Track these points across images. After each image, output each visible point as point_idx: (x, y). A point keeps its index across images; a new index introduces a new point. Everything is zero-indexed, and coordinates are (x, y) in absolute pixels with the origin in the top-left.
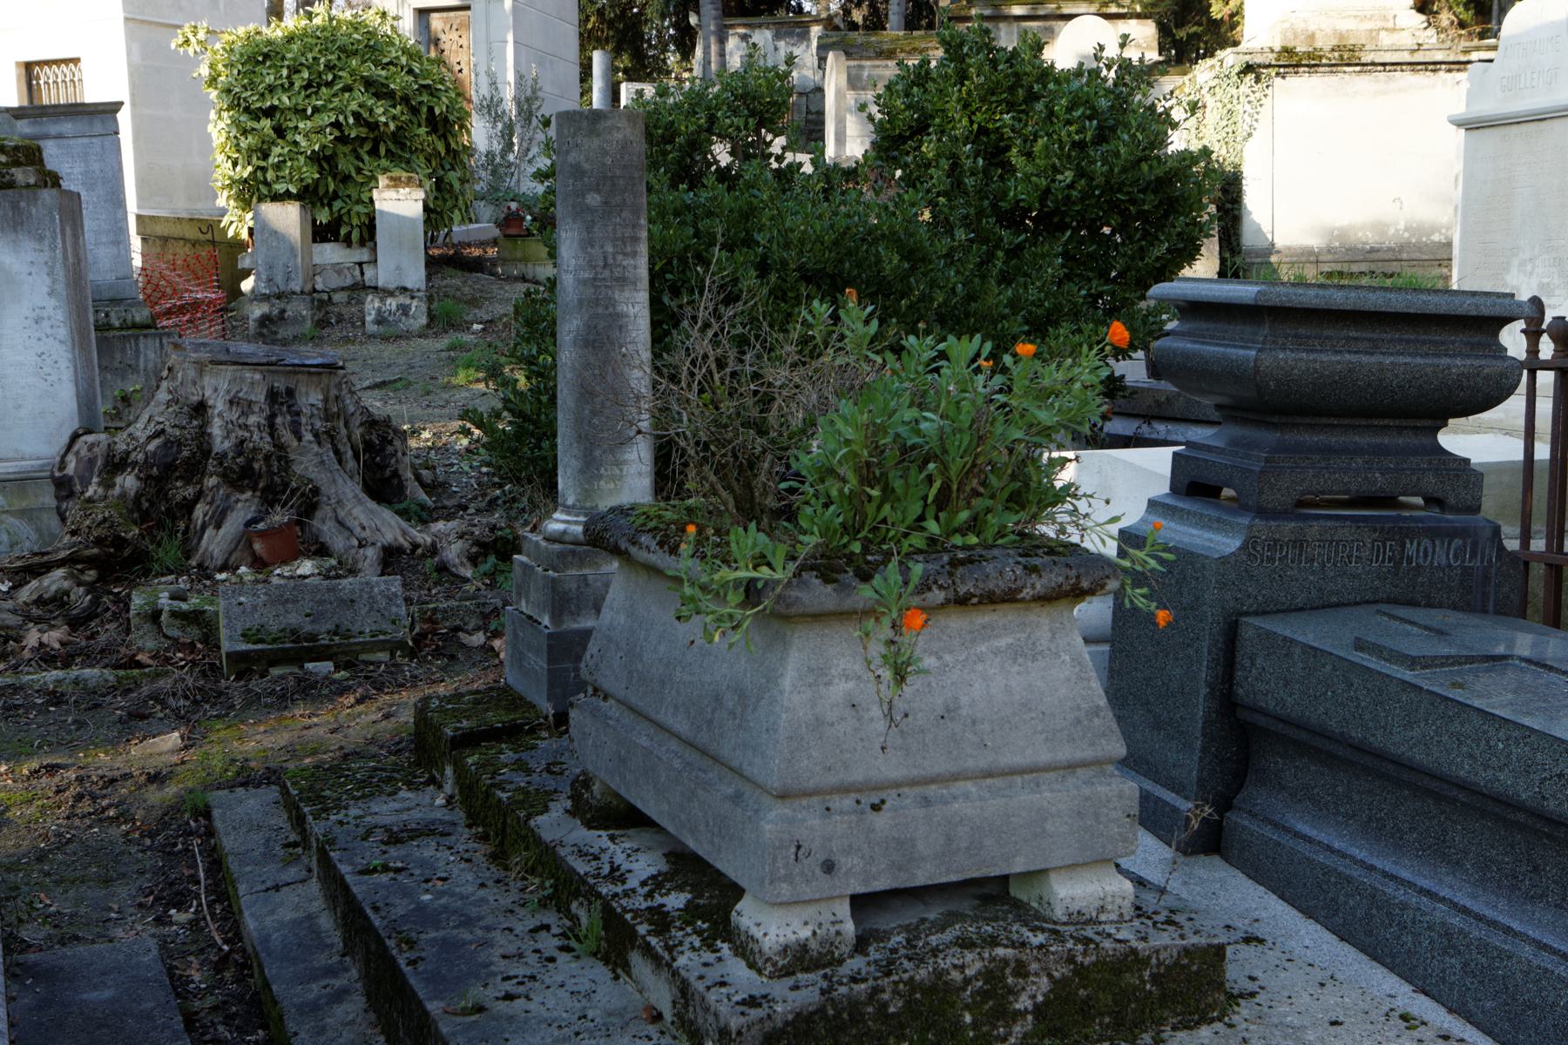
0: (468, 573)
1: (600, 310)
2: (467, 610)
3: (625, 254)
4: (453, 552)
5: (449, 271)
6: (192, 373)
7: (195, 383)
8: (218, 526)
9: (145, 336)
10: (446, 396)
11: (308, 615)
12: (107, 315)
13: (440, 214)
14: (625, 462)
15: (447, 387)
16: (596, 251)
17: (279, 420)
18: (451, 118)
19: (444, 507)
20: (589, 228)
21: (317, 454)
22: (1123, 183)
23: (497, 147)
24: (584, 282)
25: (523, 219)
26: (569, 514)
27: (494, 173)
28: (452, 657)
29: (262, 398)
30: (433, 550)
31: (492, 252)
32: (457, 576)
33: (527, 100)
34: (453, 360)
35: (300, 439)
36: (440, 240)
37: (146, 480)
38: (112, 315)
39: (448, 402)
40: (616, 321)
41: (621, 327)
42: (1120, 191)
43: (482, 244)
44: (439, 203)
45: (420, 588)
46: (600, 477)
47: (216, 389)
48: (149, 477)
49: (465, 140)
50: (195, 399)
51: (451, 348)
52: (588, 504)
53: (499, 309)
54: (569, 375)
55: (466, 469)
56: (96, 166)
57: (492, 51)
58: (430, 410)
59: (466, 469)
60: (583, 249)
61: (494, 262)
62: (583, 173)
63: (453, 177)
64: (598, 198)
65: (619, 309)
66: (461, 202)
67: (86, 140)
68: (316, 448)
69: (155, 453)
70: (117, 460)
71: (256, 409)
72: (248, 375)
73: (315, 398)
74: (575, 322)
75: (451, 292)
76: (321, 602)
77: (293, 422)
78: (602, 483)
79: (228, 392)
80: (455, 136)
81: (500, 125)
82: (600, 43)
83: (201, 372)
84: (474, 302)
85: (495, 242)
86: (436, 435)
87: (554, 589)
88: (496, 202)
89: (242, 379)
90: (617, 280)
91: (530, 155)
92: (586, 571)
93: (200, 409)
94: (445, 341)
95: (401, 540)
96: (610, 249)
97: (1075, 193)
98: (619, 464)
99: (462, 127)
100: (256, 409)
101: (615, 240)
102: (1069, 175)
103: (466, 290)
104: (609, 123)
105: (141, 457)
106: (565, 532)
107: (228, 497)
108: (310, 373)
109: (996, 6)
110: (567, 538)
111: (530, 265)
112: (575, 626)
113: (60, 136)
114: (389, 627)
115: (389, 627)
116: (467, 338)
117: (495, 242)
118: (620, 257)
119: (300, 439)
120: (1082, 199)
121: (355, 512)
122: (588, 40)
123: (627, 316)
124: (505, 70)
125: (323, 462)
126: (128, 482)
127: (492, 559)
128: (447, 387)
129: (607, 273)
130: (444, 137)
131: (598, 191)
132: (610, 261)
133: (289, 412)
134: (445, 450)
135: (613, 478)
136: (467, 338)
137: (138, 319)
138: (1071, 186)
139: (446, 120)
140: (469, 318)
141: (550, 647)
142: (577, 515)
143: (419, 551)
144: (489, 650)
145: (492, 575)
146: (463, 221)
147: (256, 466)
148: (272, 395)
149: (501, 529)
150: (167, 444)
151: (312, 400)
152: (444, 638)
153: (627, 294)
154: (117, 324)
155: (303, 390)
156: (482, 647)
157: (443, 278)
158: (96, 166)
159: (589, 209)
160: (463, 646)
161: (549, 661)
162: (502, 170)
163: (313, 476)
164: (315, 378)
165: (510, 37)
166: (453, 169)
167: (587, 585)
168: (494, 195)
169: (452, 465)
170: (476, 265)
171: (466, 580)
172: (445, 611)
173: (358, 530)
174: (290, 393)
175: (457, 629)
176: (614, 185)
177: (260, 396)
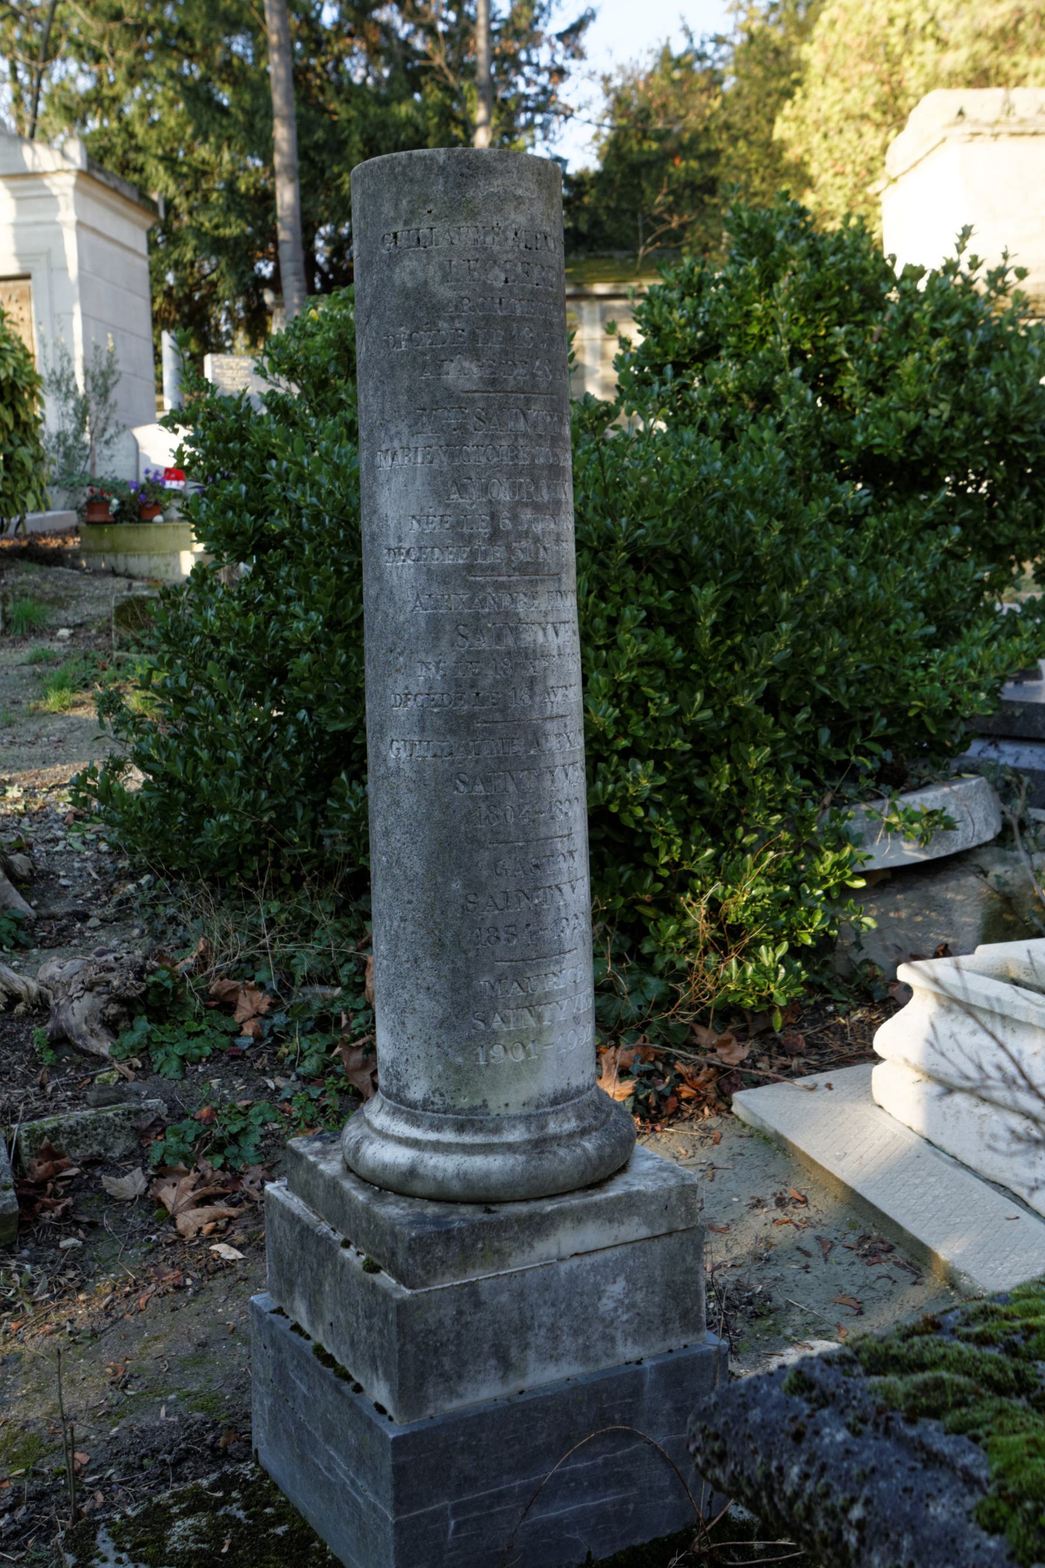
0: (103, 1046)
1: (484, 644)
2: (111, 1127)
3: (538, 508)
4: (77, 1013)
5: (23, 565)
10: (34, 728)
13: (11, 498)
14: (547, 998)
15: (35, 714)
16: (471, 501)
18: (20, 383)
19: (53, 917)
20: (454, 444)
22: (1022, 419)
23: (70, 427)
24: (444, 577)
25: (108, 503)
26: (414, 1121)
27: (66, 455)
28: (93, 1226)
30: (41, 1007)
31: (73, 543)
32: (85, 1053)
33: (102, 374)
34: (40, 677)
36: (11, 530)
39: (38, 737)
40: (522, 664)
41: (532, 682)
42: (1018, 430)
43: (57, 534)
44: (9, 484)
45: (26, 1080)
46: (491, 1038)
49: (37, 411)
51: (36, 660)
52: (464, 1102)
53: (89, 609)
54: (408, 800)
55: (77, 845)
57: (58, 320)
58: (15, 750)
59: (77, 845)
60: (439, 494)
61: (76, 554)
62: (435, 309)
63: (24, 453)
64: (474, 369)
65: (527, 638)
66: (35, 484)
74: (421, 674)
75: (29, 590)
78: (497, 1050)
80: (24, 405)
81: (72, 403)
82: (168, 325)
84: (58, 602)
85: (76, 531)
86: (30, 792)
87: (401, 1327)
88: (72, 488)
90: (522, 569)
91: (107, 436)
94: (26, 652)
96: (504, 495)
97: (957, 434)
98: (532, 1004)
99: (33, 394)
101: (514, 472)
102: (945, 409)
103: (47, 587)
104: (497, 185)
106: (412, 1172)
109: (578, 285)
110: (417, 1186)
111: (121, 557)
112: (453, 1405)
116: (56, 646)
117: (76, 531)
118: (527, 515)
120: (965, 444)
122: (159, 321)
123: (545, 656)
124: (73, 345)
127: (142, 1024)
128: (35, 714)
129: (499, 553)
130: (11, 406)
131: (476, 355)
132: (506, 524)
134: (43, 816)
136: (56, 646)
138: (951, 423)
139: (13, 386)
140: (53, 621)
141: (399, 1470)
142: (438, 1128)
143: (20, 1008)
144: (152, 1203)
145: (144, 1051)
146: (38, 508)
149: (153, 972)
152: (74, 1186)
153: (542, 603)
156: (143, 1197)
157: (19, 574)
159: (455, 399)
160: (110, 1199)
161: (400, 1503)
162: (76, 453)
165: (77, 309)
166: (24, 444)
167: (478, 1304)
168: (68, 482)
169: (56, 840)
170: (55, 558)
171: (101, 1061)
172: (73, 1131)
175: (93, 1162)
176: (509, 339)
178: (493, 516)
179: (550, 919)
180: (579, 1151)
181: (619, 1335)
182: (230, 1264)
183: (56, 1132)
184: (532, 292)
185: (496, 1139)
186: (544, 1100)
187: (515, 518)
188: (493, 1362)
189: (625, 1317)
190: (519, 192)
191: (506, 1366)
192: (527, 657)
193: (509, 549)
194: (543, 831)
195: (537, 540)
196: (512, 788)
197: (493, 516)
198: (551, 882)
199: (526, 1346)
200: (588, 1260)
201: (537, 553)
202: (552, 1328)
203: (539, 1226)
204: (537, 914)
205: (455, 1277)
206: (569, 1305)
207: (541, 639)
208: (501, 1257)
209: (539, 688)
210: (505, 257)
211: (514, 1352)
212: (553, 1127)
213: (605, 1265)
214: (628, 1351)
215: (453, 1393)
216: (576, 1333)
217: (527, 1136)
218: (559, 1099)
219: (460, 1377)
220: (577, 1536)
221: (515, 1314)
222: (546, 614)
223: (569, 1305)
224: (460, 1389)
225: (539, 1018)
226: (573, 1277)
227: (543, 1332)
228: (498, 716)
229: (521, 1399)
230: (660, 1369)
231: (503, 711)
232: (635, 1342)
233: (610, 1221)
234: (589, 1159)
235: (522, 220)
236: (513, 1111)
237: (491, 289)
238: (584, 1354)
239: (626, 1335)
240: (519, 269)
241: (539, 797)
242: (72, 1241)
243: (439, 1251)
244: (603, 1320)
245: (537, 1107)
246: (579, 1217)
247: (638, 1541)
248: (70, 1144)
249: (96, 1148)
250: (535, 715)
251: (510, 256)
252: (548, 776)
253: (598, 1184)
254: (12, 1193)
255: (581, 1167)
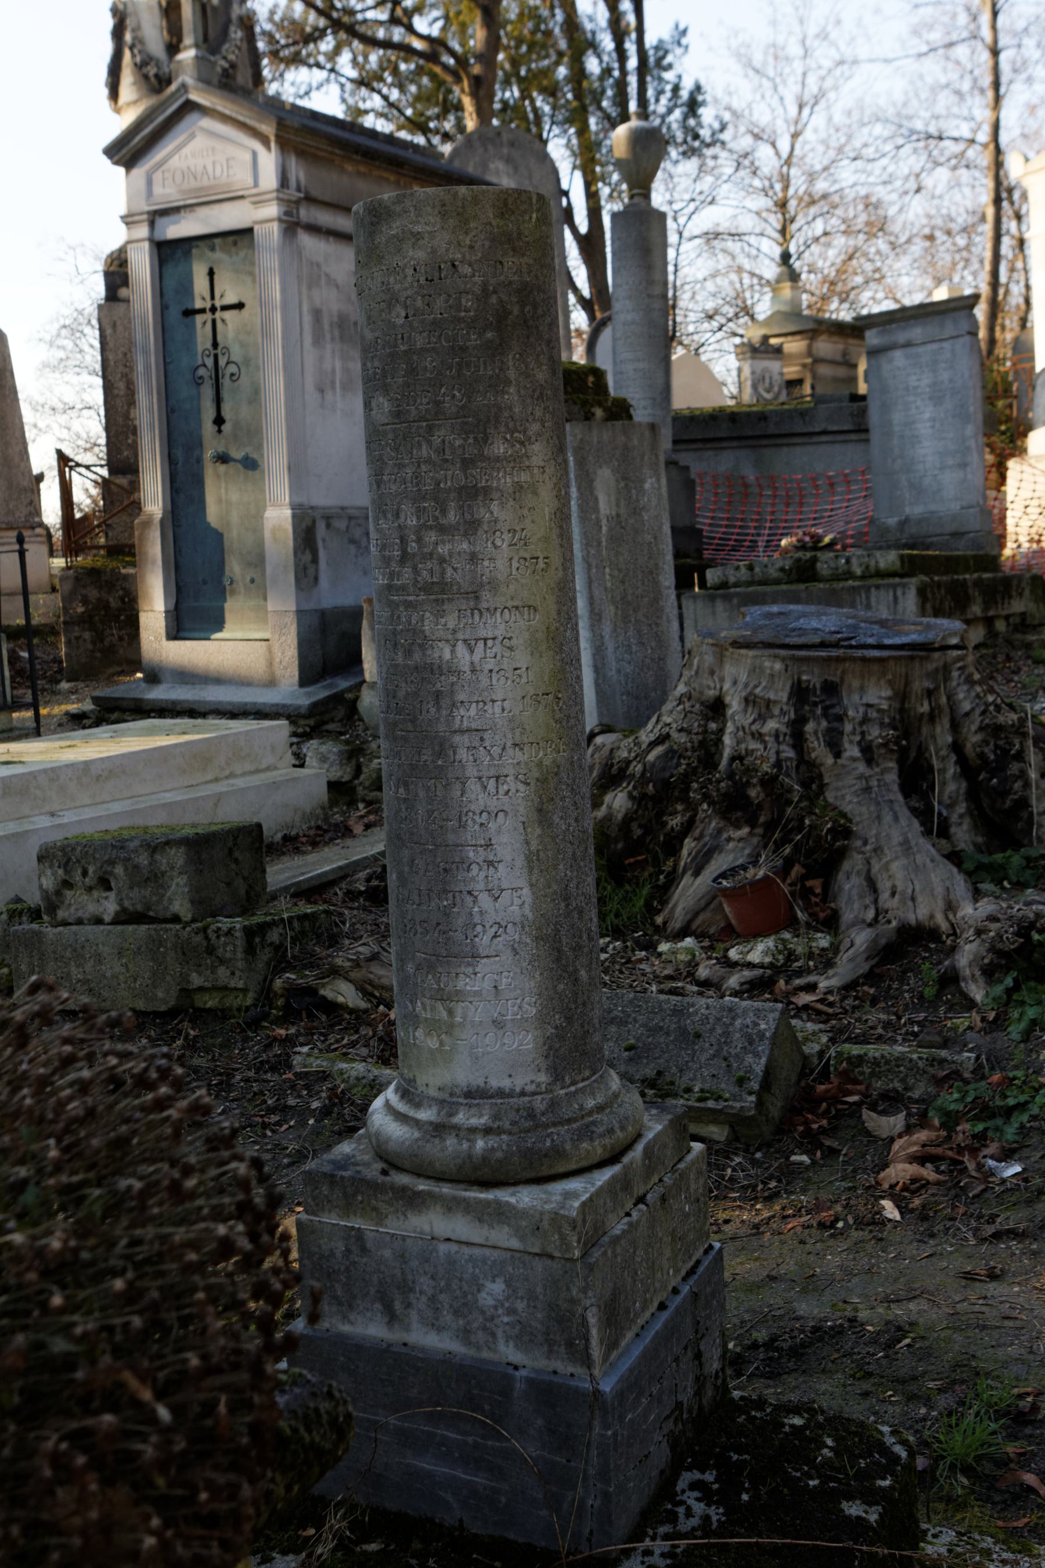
2: (912, 1066)
3: (442, 529)
6: (709, 659)
7: (712, 673)
8: (697, 874)
9: (878, 587)
11: (629, 1049)
12: (848, 561)
14: (458, 996)
17: (810, 727)
21: (860, 777)
29: (784, 696)
32: (965, 996)
35: (837, 755)
37: (639, 800)
38: (854, 561)
41: (438, 696)
47: (735, 679)
48: (644, 796)
50: (712, 693)
56: (945, 376)
67: (935, 346)
68: (861, 767)
69: (653, 765)
70: (614, 770)
71: (776, 711)
72: (767, 664)
73: (878, 694)
76: (655, 1030)
77: (829, 731)
78: (420, 1033)
79: (746, 685)
83: (721, 659)
89: (762, 669)
92: (357, 1223)
93: (717, 708)
95: (940, 918)
96: (412, 522)
98: (447, 997)
100: (776, 711)
105: (639, 768)
107: (719, 831)
108: (864, 659)
112: (346, 1328)
113: (908, 345)
114: (727, 1087)
115: (727, 1087)
118: (431, 537)
119: (837, 755)
121: (895, 866)
125: (868, 789)
126: (618, 801)
129: (407, 573)
132: (413, 547)
133: (825, 715)
135: (434, 1027)
137: (882, 565)
147: (753, 793)
148: (800, 693)
150: (670, 754)
151: (871, 698)
154: (858, 571)
155: (856, 683)
158: (945, 376)
160: (868, 1133)
163: (847, 809)
164: (875, 667)
167: (364, 1250)
172: (876, 1063)
173: (884, 896)
174: (831, 689)
176: (412, 371)
177: (781, 694)
178: (403, 540)
179: (460, 921)
180: (465, 1145)
181: (500, 1334)
182: (884, 1222)
183: (861, 1059)
184: (434, 322)
185: (412, 1113)
186: (457, 1091)
187: (419, 540)
188: (378, 1306)
189: (506, 1319)
190: (419, 228)
191: (392, 1317)
192: (432, 672)
193: (416, 571)
194: (451, 838)
195: (442, 560)
196: (422, 794)
197: (403, 540)
198: (461, 887)
199: (409, 1305)
200: (466, 1250)
201: (443, 572)
202: (433, 1299)
203: (413, 1201)
204: (447, 915)
205: (341, 1218)
206: (448, 1285)
207: (447, 655)
208: (380, 1219)
209: (445, 702)
210: (405, 294)
211: (398, 1306)
212: (460, 1118)
213: (484, 1261)
214: (509, 1352)
215: (345, 1318)
216: (456, 1313)
217: (433, 1118)
218: (475, 1095)
219: (351, 1307)
220: (449, 1498)
221: (398, 1272)
222: (454, 631)
223: (448, 1285)
224: (352, 1317)
225: (451, 1013)
226: (451, 1261)
227: (424, 1299)
228: (410, 727)
229: (404, 1350)
230: (530, 1382)
231: (413, 721)
232: (516, 1346)
233: (481, 1221)
234: (470, 1157)
235: (421, 255)
236: (432, 1092)
237: (394, 326)
238: (465, 1335)
239: (508, 1339)
240: (419, 303)
241: (447, 806)
242: (805, 1158)
243: (325, 1190)
244: (483, 1312)
245: (451, 1095)
246: (451, 1206)
247: (511, 1536)
248: (873, 1074)
249: (898, 1085)
250: (441, 727)
251: (409, 292)
252: (458, 786)
253: (486, 1184)
254: (753, 1098)
255: (459, 1161)
